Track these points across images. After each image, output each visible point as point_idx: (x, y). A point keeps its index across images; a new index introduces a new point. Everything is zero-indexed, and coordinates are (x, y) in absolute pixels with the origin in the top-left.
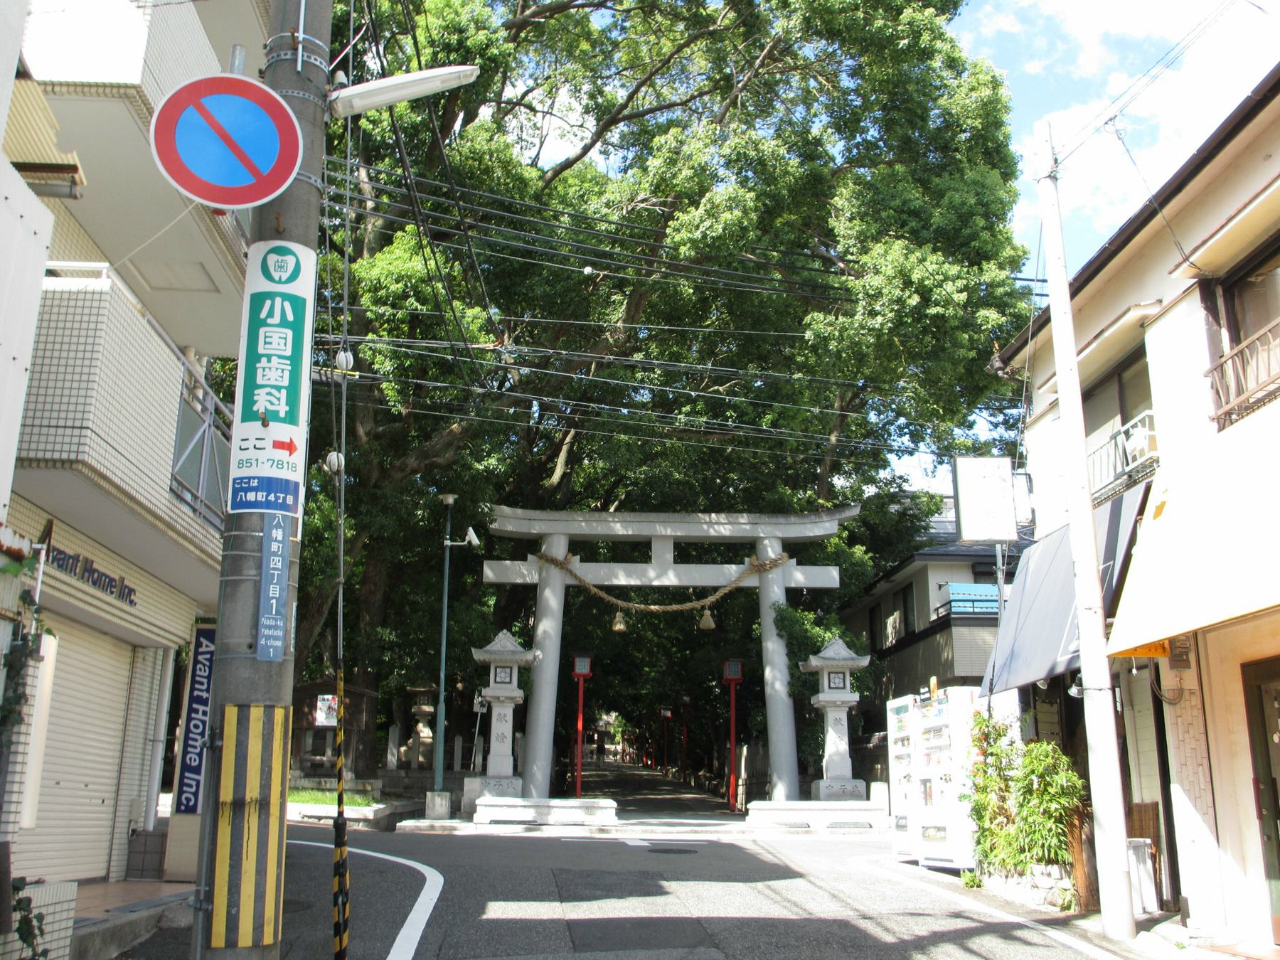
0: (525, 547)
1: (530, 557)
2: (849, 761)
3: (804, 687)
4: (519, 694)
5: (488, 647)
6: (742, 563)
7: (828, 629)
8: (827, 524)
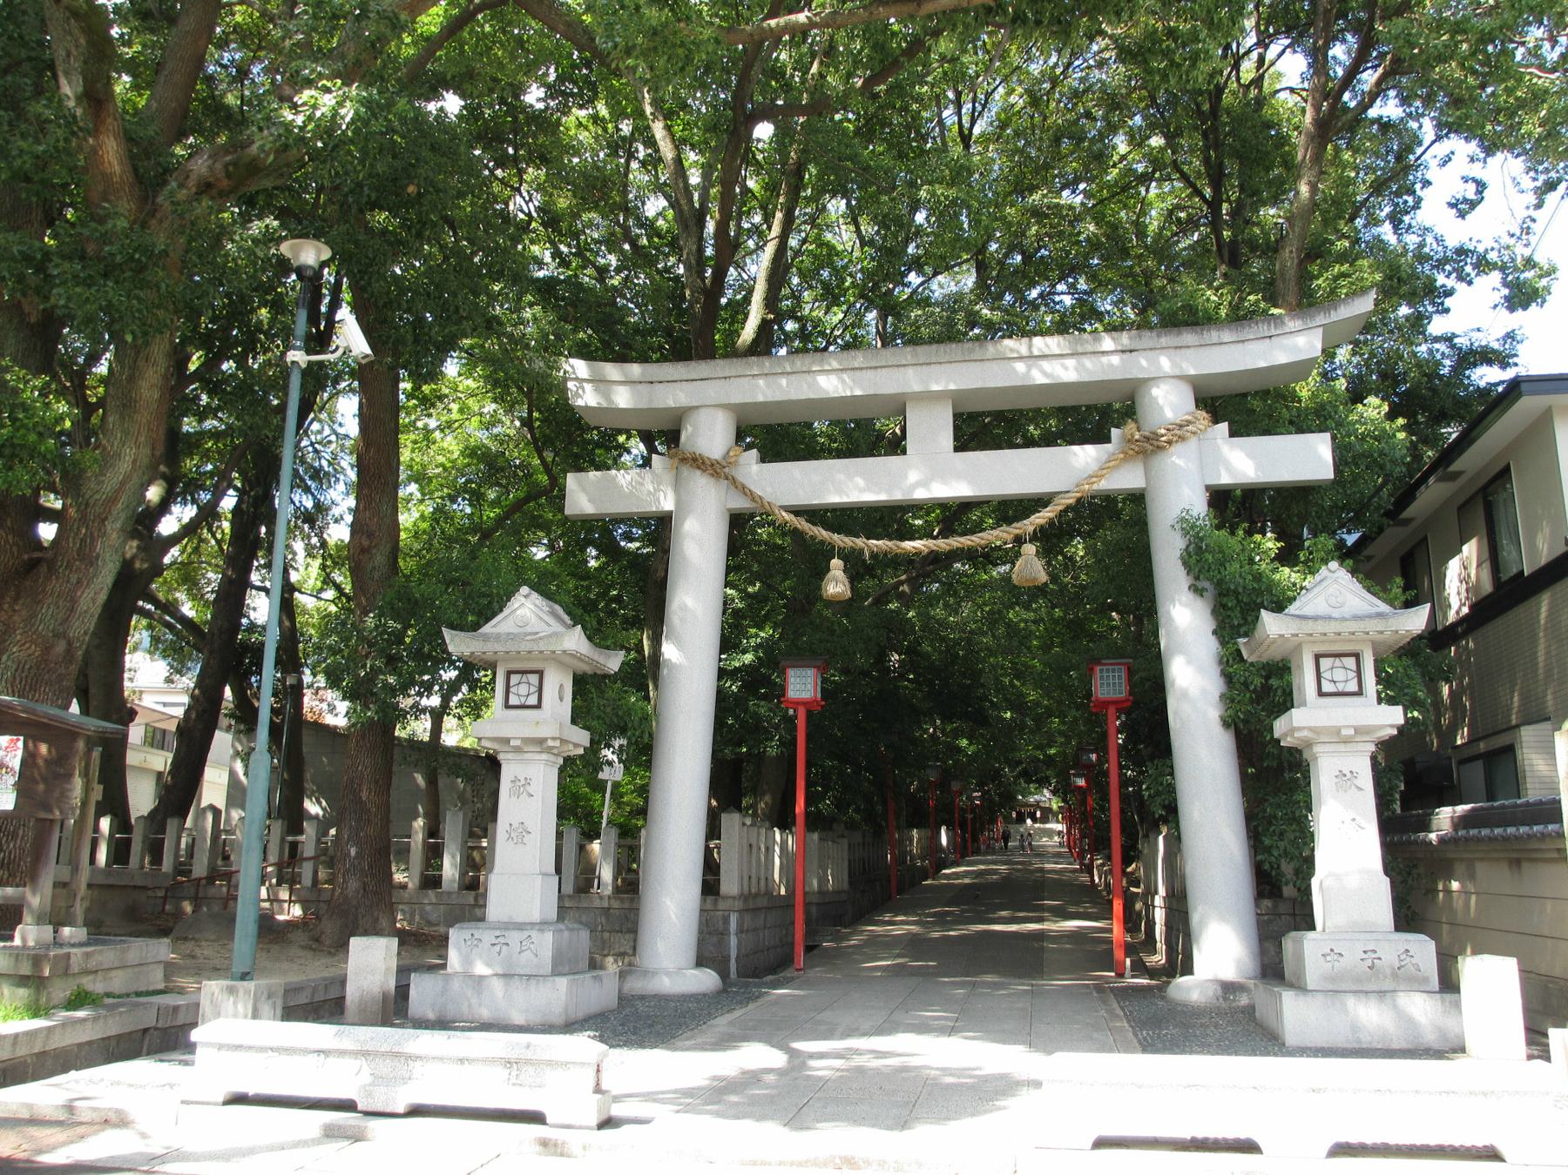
2: (1385, 882)
3: (1258, 693)
5: (487, 629)
8: (1301, 340)
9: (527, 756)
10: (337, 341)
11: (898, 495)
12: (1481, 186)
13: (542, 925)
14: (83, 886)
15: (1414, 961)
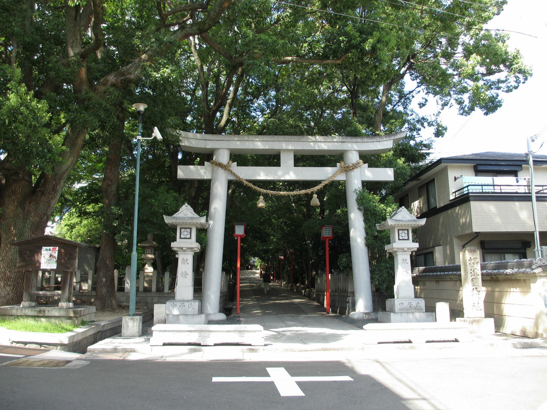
0: (206, 157)
1: (206, 163)
3: (378, 242)
4: (197, 246)
5: (175, 215)
6: (335, 166)
7: (387, 205)
8: (385, 142)
9: (187, 252)
10: (154, 135)
11: (276, 178)
12: (426, 101)
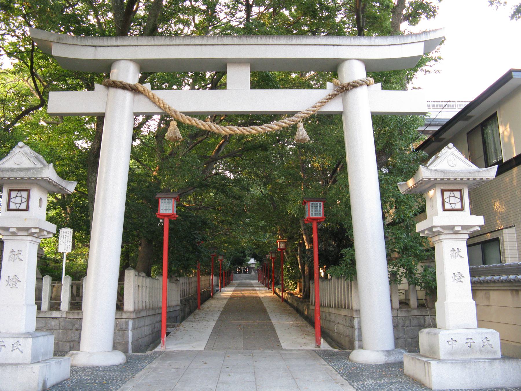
13: (27, 335)
14: (302, 227)
15: (490, 343)
